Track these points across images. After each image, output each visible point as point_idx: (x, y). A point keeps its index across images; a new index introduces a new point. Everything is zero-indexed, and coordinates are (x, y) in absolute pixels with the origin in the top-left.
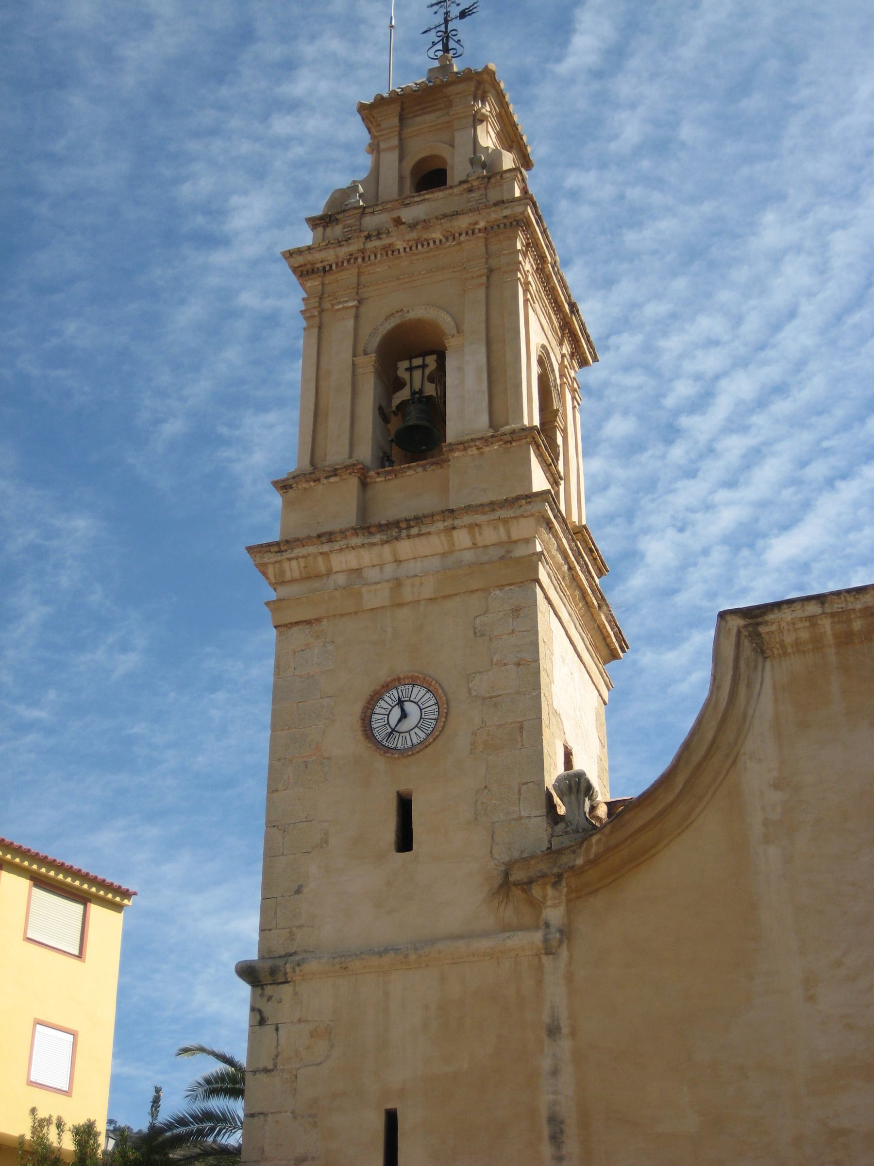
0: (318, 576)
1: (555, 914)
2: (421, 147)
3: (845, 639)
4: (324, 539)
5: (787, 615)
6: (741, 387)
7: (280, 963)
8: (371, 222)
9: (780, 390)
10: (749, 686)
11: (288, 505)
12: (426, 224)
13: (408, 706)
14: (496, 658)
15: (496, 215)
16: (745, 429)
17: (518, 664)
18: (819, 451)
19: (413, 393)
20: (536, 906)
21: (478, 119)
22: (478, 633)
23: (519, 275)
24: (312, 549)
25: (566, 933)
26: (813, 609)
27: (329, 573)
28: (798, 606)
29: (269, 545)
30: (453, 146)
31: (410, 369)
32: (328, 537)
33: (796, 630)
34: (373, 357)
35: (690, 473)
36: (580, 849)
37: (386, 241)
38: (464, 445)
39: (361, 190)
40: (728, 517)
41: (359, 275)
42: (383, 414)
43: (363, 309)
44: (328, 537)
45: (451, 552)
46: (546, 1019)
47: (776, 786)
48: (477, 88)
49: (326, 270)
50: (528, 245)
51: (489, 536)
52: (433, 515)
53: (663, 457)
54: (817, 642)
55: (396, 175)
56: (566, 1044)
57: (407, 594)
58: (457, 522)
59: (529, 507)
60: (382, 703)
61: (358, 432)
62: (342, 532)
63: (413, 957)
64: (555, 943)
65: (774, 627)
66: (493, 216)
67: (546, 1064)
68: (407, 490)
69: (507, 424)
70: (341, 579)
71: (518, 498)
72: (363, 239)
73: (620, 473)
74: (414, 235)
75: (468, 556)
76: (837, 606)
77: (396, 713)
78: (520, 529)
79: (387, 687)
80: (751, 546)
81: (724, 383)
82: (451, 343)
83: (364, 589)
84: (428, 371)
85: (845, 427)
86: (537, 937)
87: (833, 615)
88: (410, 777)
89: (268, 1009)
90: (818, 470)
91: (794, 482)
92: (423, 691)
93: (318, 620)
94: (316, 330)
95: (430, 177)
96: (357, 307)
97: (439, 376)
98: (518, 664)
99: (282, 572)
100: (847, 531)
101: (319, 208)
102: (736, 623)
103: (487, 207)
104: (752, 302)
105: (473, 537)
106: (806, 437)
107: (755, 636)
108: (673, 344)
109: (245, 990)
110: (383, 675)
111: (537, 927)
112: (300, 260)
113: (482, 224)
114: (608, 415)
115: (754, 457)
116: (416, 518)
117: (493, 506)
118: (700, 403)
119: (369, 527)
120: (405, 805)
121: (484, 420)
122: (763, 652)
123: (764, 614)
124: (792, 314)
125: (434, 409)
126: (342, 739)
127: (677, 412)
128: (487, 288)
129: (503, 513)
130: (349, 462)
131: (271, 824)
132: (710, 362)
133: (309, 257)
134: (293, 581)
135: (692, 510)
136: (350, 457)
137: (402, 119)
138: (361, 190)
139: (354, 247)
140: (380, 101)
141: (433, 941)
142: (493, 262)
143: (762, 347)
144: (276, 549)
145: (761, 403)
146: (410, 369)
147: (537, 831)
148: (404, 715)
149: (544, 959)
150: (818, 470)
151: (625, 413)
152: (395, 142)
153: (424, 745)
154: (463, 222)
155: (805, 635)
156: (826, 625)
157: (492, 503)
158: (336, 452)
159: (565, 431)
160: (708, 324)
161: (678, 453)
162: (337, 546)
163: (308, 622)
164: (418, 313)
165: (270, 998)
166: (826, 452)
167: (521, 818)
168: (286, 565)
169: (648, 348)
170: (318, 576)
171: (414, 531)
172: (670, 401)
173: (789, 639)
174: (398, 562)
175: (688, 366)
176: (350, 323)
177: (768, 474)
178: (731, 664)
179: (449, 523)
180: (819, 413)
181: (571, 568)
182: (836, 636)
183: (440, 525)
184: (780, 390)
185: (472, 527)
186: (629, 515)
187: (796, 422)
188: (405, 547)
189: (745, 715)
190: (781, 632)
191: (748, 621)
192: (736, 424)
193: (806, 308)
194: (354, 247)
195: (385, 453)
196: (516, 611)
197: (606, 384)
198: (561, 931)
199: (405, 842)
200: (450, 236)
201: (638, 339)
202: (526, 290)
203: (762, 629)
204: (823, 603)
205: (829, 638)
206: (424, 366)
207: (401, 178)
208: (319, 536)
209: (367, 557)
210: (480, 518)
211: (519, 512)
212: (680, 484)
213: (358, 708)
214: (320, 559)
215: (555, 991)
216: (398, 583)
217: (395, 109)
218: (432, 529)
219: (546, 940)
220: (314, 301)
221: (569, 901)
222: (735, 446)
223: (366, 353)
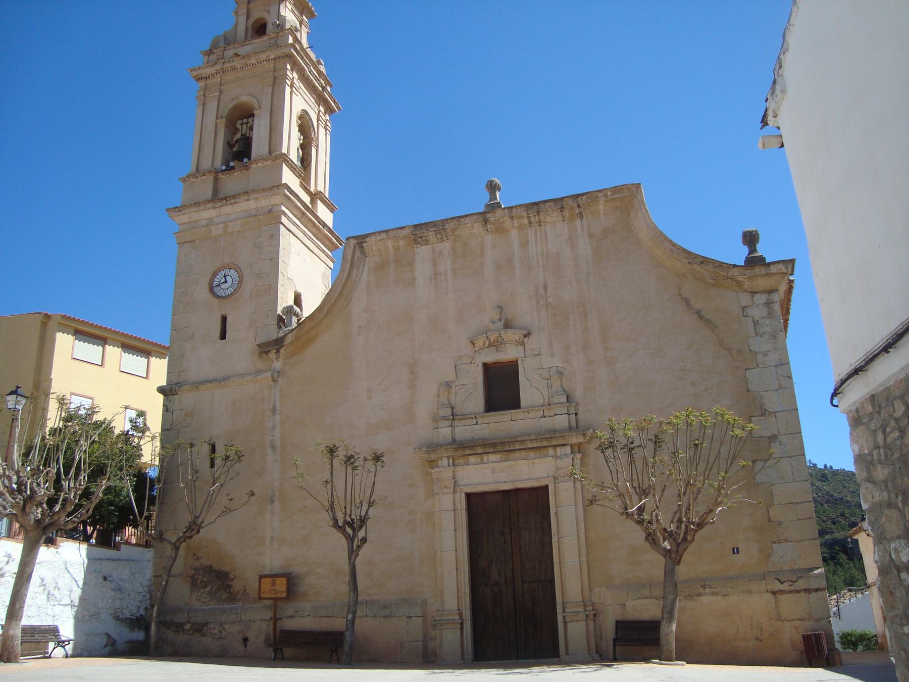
5: (373, 238)
12: (248, 56)
13: (228, 278)
15: (279, 52)
19: (242, 135)
31: (242, 124)
32: (197, 204)
34: (224, 120)
36: (286, 337)
37: (232, 64)
43: (222, 96)
47: (365, 311)
71: (274, 187)
74: (244, 61)
77: (223, 280)
79: (219, 270)
95: (260, 29)
97: (251, 129)
102: (353, 242)
109: (161, 397)
112: (195, 73)
113: (272, 57)
119: (217, 197)
120: (224, 319)
125: (247, 142)
126: (202, 293)
131: (173, 329)
133: (199, 72)
139: (219, 67)
146: (242, 124)
154: (263, 56)
159: (317, 147)
182: (394, 247)
194: (219, 67)
199: (223, 336)
202: (292, 86)
206: (247, 123)
207: (247, 28)
210: (258, 195)
213: (208, 279)
218: (239, 200)
219: (272, 376)
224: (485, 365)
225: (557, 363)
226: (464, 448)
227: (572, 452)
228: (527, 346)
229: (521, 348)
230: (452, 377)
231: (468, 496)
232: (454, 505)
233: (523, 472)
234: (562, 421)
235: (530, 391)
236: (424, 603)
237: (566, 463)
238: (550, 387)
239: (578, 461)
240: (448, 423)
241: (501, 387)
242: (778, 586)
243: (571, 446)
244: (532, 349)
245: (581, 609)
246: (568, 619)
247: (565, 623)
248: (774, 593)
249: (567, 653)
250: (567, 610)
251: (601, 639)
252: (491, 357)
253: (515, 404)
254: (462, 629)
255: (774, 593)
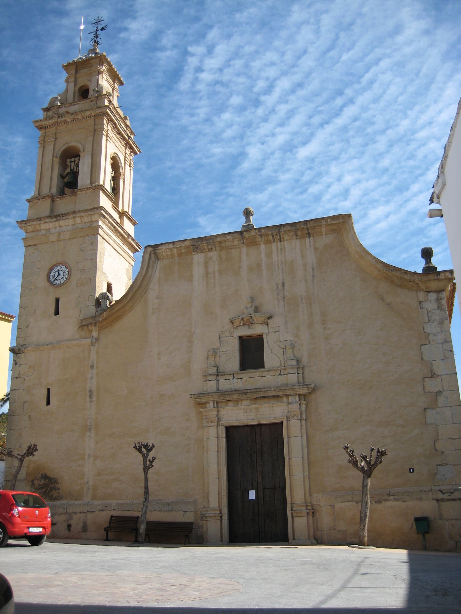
0: (38, 231)
1: (95, 334)
2: (82, 82)
3: (180, 255)
4: (38, 220)
5: (164, 247)
6: (284, 84)
7: (21, 347)
8: (62, 111)
9: (300, 85)
10: (153, 268)
11: (30, 207)
13: (60, 272)
14: (85, 258)
15: (97, 111)
16: (287, 102)
17: (91, 260)
18: (316, 112)
19: (71, 170)
20: (90, 331)
21: (100, 73)
22: (81, 250)
23: (104, 132)
24: (35, 223)
25: (97, 340)
26: (171, 246)
27: (41, 230)
28: (167, 245)
29: (23, 221)
30: (91, 82)
31: (71, 162)
32: (39, 219)
33: (167, 252)
34: (58, 158)
35: (265, 120)
37: (64, 119)
38: (81, 190)
39: (59, 98)
40: (281, 139)
41: (56, 130)
42: (62, 176)
44: (39, 219)
45: (75, 224)
46: (90, 363)
47: (157, 298)
48: (100, 61)
49: (46, 128)
50: (109, 121)
51: (86, 220)
52: (69, 213)
53: (254, 113)
54: (173, 256)
55: (73, 92)
56: (95, 370)
57: (62, 237)
58: (77, 215)
59: (97, 211)
60: (53, 271)
61: (52, 184)
62: (43, 217)
63: (56, 346)
64: (94, 342)
65: (160, 251)
66: (97, 112)
67: (89, 376)
68: (64, 205)
69: (95, 183)
70: (44, 232)
72: (57, 118)
73: (238, 119)
74: (72, 117)
75: (80, 226)
76: (177, 245)
77: (57, 273)
78: (95, 218)
79: (55, 266)
80: (291, 151)
81: (278, 82)
82: (81, 154)
83: (50, 235)
84: (76, 163)
85: (327, 102)
86: (89, 340)
87: (177, 248)
88: (60, 293)
89: (17, 360)
90: (316, 120)
91: (307, 124)
92: (65, 267)
93: (37, 244)
94: (42, 148)
95: (84, 93)
96: (55, 141)
97: (78, 165)
98: (91, 260)
99: (27, 229)
100: (330, 145)
101: (46, 105)
102: (150, 249)
103: (95, 109)
104: (289, 46)
105: (81, 220)
106: (311, 106)
107: (155, 253)
108: (256, 64)
110: (54, 262)
111: (90, 338)
112: (38, 124)
113: (93, 114)
114: (231, 95)
115: (291, 114)
116: (65, 214)
117: (87, 211)
118: (269, 90)
119: (54, 216)
121: (89, 181)
122: (158, 258)
123: (157, 247)
124: (305, 52)
126: (42, 282)
127: (259, 94)
128: (94, 136)
129: (90, 213)
130: (50, 194)
132: (272, 72)
134: (30, 232)
135: (267, 136)
136: (50, 191)
137: (76, 70)
138: (59, 98)
139: (54, 120)
140: (69, 65)
141: (62, 341)
142: (96, 127)
143: (294, 66)
144: (24, 222)
145: (293, 91)
146: (71, 162)
147: (92, 309)
148: (59, 275)
149: (91, 346)
150: (316, 120)
151: (238, 94)
152: (73, 79)
153: (64, 284)
154: (87, 113)
155: (169, 253)
156: (175, 251)
157: (86, 210)
158: (45, 191)
160: (271, 56)
161: (260, 112)
162: (42, 222)
163: (34, 245)
164: (73, 144)
165: (18, 357)
166: (320, 112)
167: (88, 306)
168: (28, 227)
169: (247, 66)
170: (38, 231)
171: (64, 218)
172: (256, 89)
173: (165, 254)
174: (60, 227)
175: (263, 74)
176: (52, 146)
177: (297, 121)
178: (147, 262)
179: (74, 215)
180: (317, 95)
181: (115, 227)
182: (178, 254)
183: (72, 216)
184: (300, 85)
185: (81, 217)
186: (242, 137)
187: (307, 99)
188: (62, 223)
189: (150, 277)
190: (162, 252)
191: (153, 249)
192: (283, 100)
193: (311, 49)
194: (54, 120)
195: (62, 190)
196: (92, 243)
197: (230, 81)
198: (96, 339)
199: (57, 313)
200: (84, 118)
201: (242, 61)
203: (157, 251)
204: (174, 244)
205: (176, 254)
206: (75, 161)
207: (75, 92)
208: (37, 219)
209: (51, 225)
210: (83, 214)
211: (94, 212)
212: (261, 125)
213: (46, 272)
214: (38, 226)
215: (93, 356)
216: (59, 234)
217: (74, 67)
218: (69, 217)
219: (91, 342)
220: (42, 138)
221: (99, 330)
222: (283, 109)
223: (56, 157)
224: (240, 337)
225: (289, 337)
226: (224, 397)
227: (300, 400)
228: (269, 325)
229: (265, 327)
230: (218, 345)
231: (228, 429)
232: (218, 434)
233: (269, 413)
234: (293, 378)
235: (271, 357)
236: (196, 502)
237: (295, 407)
238: (285, 354)
239: (303, 406)
240: (215, 377)
241: (251, 353)
242: (441, 496)
243: (299, 395)
244: (274, 328)
245: (304, 508)
246: (294, 515)
247: (293, 517)
248: (438, 500)
249: (294, 539)
250: (294, 509)
251: (317, 530)
252: (245, 332)
253: (261, 365)
254: (221, 520)
255: (438, 500)
